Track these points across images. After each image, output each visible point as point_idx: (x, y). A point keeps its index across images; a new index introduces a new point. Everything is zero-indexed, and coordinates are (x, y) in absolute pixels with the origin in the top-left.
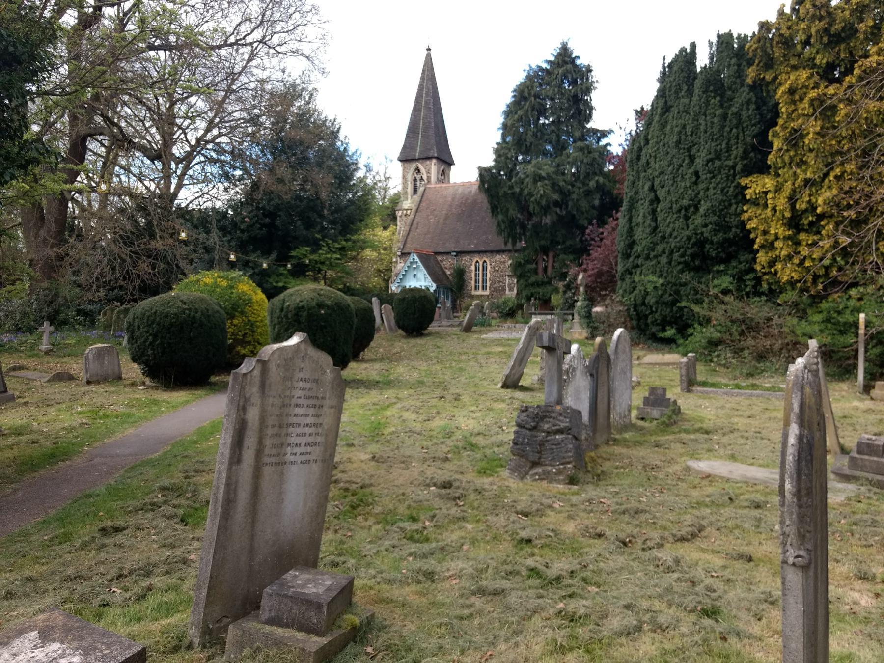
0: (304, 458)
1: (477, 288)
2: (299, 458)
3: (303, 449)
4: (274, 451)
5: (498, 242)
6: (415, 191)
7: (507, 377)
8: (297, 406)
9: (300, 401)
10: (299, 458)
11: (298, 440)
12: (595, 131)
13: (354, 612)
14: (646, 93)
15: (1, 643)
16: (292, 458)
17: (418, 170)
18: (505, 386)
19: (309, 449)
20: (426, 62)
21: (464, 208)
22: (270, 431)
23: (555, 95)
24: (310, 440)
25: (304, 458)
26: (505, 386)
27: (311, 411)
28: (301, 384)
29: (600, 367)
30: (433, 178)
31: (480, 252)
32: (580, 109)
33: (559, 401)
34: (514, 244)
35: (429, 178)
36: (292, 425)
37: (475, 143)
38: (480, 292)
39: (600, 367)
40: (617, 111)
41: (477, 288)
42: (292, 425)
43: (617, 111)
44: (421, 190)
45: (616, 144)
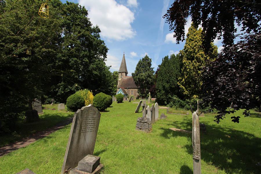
0: (91, 130)
1: (131, 94)
2: (90, 131)
3: (91, 129)
4: (84, 129)
5: (135, 86)
6: (121, 78)
7: (136, 111)
8: (90, 119)
9: (90, 118)
10: (90, 131)
11: (90, 127)
12: (152, 68)
13: (163, 131)
14: (160, 63)
15: (1, 153)
16: (88, 131)
17: (122, 74)
18: (136, 112)
19: (92, 129)
20: (122, 63)
21: (129, 79)
22: (83, 125)
23: (145, 64)
24: (92, 126)
25: (91, 130)
26: (136, 112)
27: (93, 120)
28: (91, 115)
29: (153, 111)
30: (124, 76)
31: (132, 88)
32: (150, 64)
33: (145, 117)
34: (138, 87)
35: (124, 75)
36: (88, 124)
37: (131, 70)
38: (132, 95)
39: (153, 111)
40: (155, 66)
41: (131, 94)
42: (88, 124)
43: (155, 66)
44: (122, 77)
45: (155, 70)
